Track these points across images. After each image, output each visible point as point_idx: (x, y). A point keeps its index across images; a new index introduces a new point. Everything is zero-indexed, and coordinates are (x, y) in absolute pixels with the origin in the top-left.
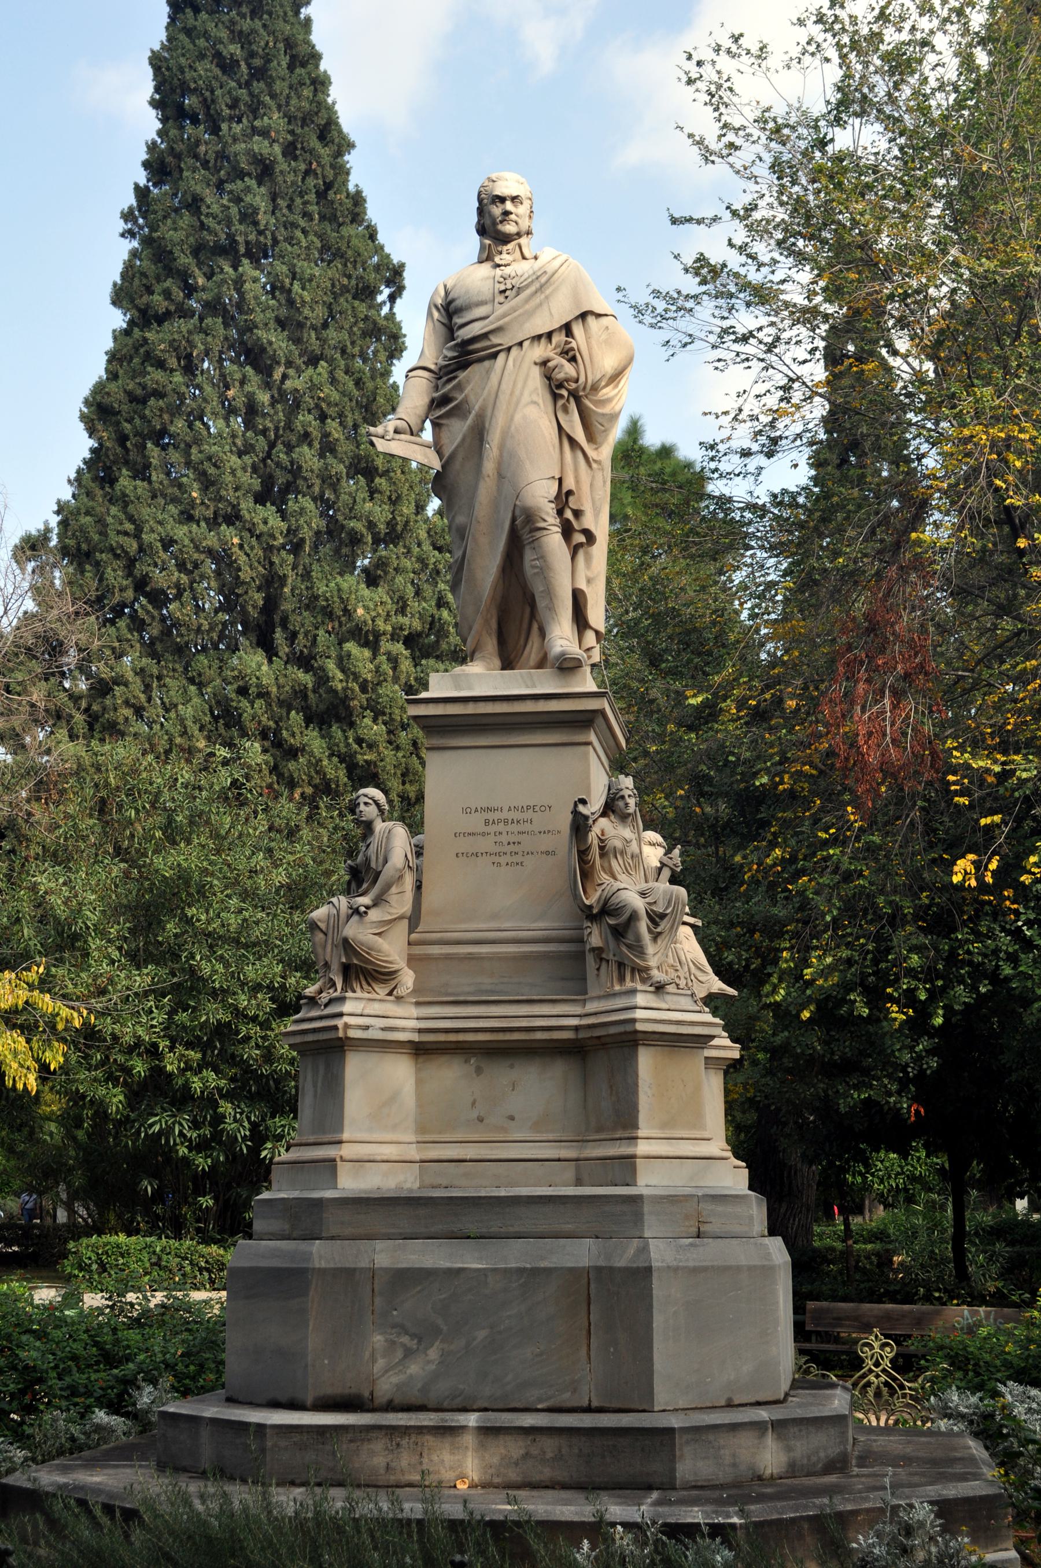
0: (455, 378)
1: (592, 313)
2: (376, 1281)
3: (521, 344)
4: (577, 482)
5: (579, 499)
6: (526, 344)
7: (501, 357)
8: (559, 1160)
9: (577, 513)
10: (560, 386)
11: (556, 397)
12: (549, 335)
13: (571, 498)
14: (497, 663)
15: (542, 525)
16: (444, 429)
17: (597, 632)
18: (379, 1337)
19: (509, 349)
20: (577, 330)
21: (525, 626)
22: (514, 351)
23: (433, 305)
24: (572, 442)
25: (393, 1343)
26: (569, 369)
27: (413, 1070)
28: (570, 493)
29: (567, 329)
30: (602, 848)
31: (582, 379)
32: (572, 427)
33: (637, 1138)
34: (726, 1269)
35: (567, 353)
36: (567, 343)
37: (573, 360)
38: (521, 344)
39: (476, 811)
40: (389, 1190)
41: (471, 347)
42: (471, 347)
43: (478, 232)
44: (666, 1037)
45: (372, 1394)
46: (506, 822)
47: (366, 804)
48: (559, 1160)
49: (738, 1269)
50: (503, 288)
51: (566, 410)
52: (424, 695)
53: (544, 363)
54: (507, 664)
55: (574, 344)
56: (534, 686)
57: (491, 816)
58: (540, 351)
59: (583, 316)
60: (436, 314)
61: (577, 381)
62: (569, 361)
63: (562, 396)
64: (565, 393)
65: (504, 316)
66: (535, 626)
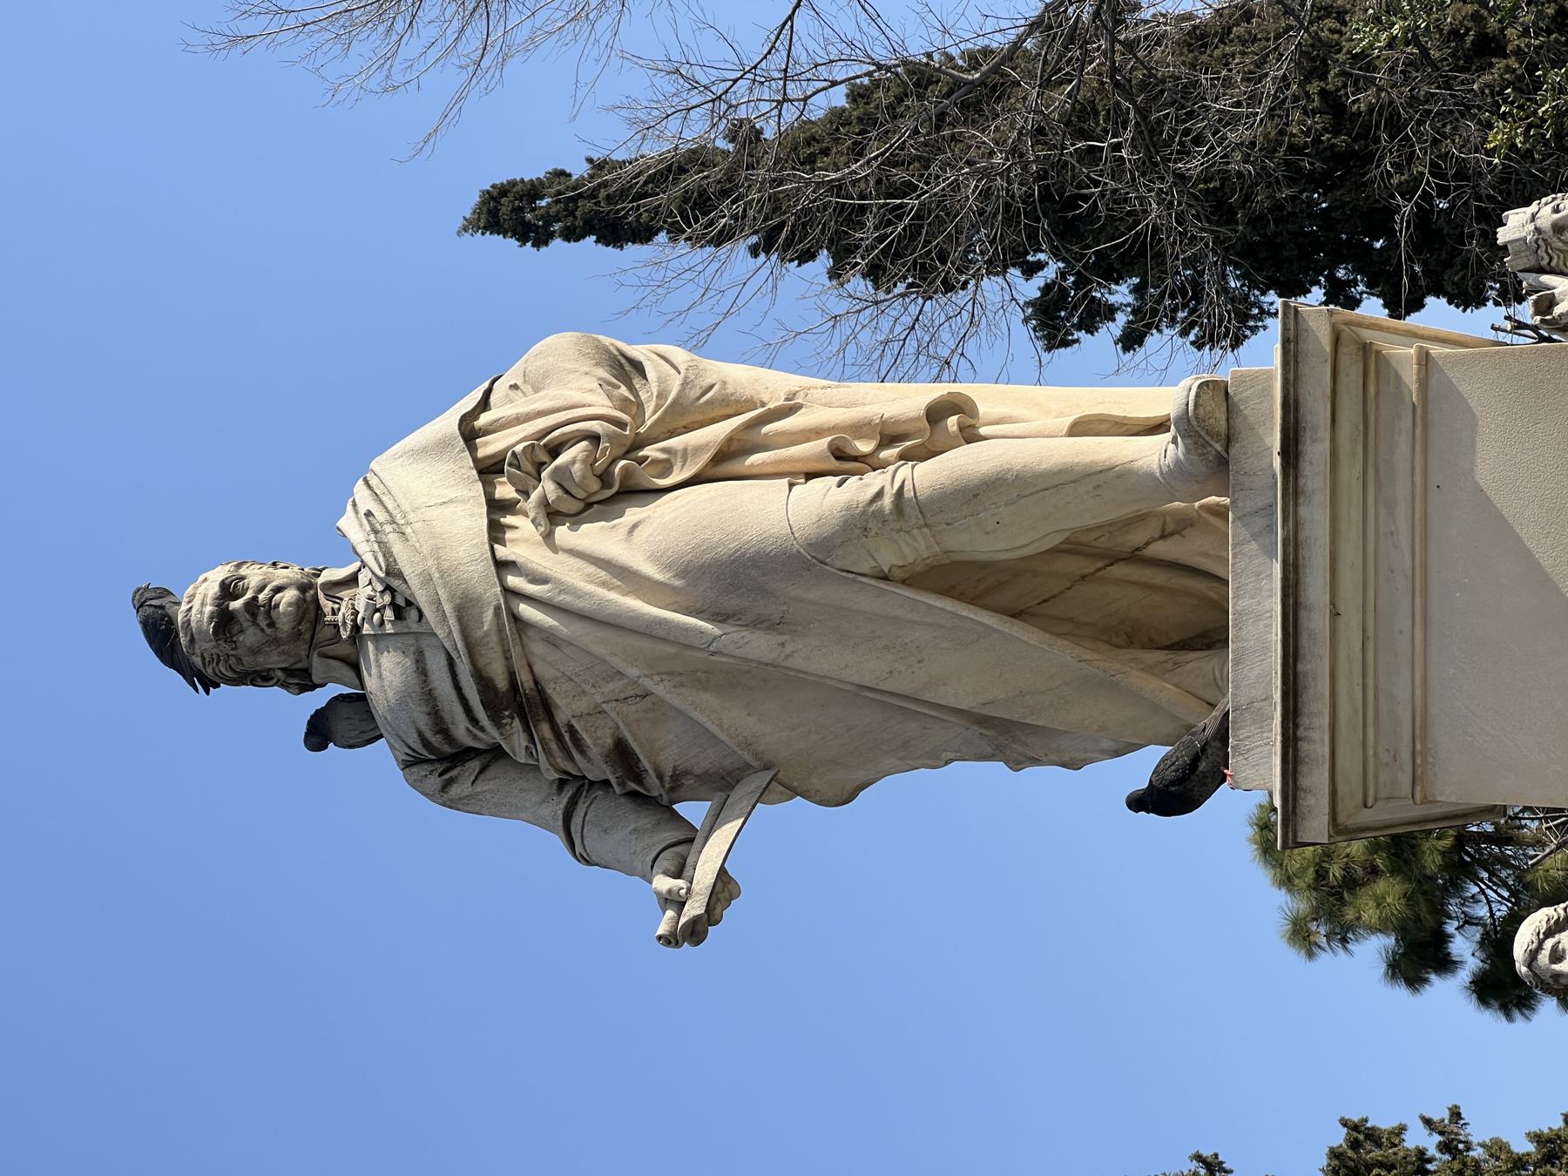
10: (605, 478)
12: (497, 507)
15: (887, 501)
23: (443, 794)
29: (489, 470)
32: (698, 450)
47: (1557, 956)
53: (553, 515)
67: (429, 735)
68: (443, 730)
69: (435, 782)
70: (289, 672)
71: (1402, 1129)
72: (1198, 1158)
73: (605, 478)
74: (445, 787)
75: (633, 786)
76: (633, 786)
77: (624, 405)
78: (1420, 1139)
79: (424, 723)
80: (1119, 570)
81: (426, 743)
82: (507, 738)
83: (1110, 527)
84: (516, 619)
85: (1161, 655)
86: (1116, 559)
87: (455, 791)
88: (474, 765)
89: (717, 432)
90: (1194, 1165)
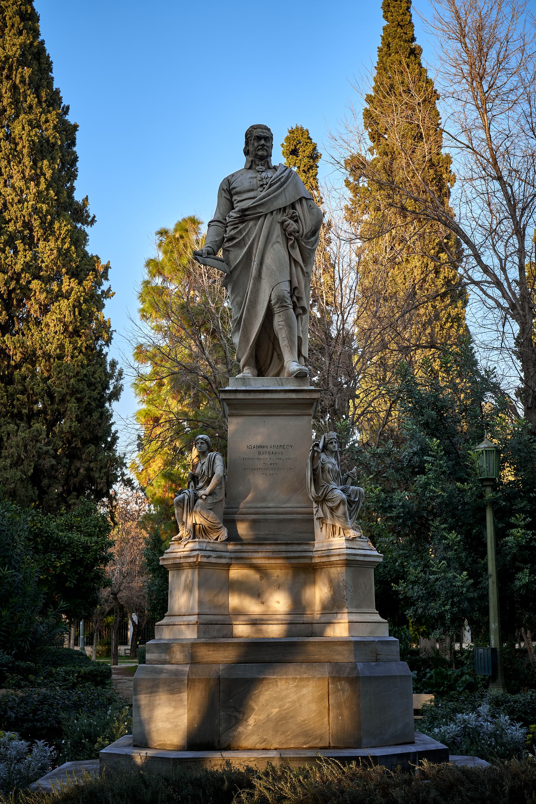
0: (237, 227)
1: (304, 197)
2: (221, 685)
3: (272, 213)
4: (299, 283)
5: (299, 292)
6: (275, 212)
7: (261, 220)
8: (303, 623)
9: (299, 299)
10: (290, 234)
11: (287, 240)
12: (285, 209)
13: (296, 292)
14: (256, 372)
16: (231, 253)
17: (305, 358)
18: (222, 713)
19: (266, 215)
20: (298, 207)
21: (270, 353)
22: (268, 216)
24: (296, 262)
25: (230, 716)
26: (294, 226)
27: (290, 577)
28: (296, 288)
30: (322, 468)
31: (301, 231)
32: (296, 255)
33: (198, 614)
34: (392, 677)
35: (293, 218)
36: (293, 213)
37: (296, 221)
38: (272, 213)
39: (254, 447)
40: (273, 638)
41: (247, 213)
42: (247, 213)
43: (245, 153)
44: (358, 563)
45: (219, 741)
46: (269, 453)
48: (303, 623)
49: (395, 677)
50: (262, 183)
51: (293, 246)
52: (227, 388)
53: (282, 223)
54: (261, 373)
55: (297, 214)
56: (283, 385)
57: (261, 450)
58: (280, 217)
59: (300, 200)
60: (224, 195)
61: (298, 232)
62: (295, 221)
63: (291, 239)
64: (293, 238)
65: (264, 197)
66: (275, 354)
67: (235, 190)
68: (237, 193)
69: (225, 188)
70: (248, 150)
71: (108, 280)
72: (94, 217)
73: (290, 234)
74: (223, 190)
75: (226, 240)
76: (226, 240)
77: (306, 236)
78: (105, 287)
79: (238, 189)
80: (271, 345)
81: (235, 188)
82: (235, 212)
83: (253, 745)
84: (261, 216)
85: (254, 353)
86: (273, 344)
87: (223, 192)
88: (229, 198)
89: (299, 259)
90: (92, 216)
